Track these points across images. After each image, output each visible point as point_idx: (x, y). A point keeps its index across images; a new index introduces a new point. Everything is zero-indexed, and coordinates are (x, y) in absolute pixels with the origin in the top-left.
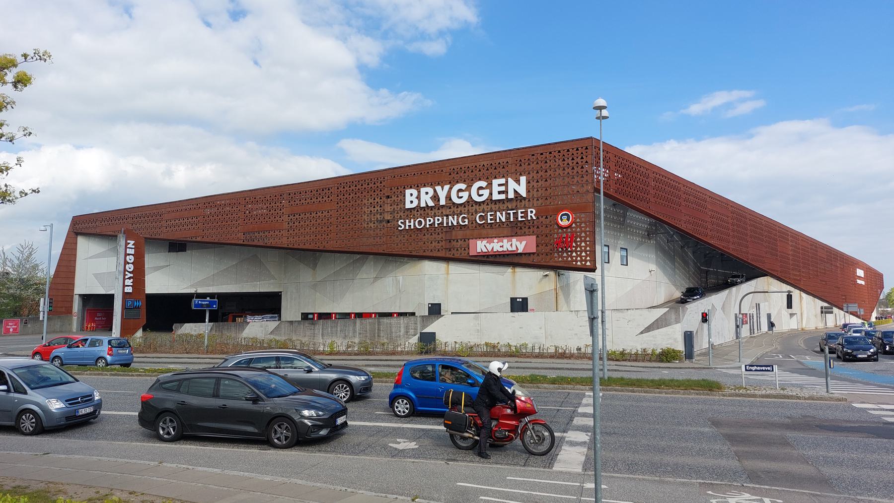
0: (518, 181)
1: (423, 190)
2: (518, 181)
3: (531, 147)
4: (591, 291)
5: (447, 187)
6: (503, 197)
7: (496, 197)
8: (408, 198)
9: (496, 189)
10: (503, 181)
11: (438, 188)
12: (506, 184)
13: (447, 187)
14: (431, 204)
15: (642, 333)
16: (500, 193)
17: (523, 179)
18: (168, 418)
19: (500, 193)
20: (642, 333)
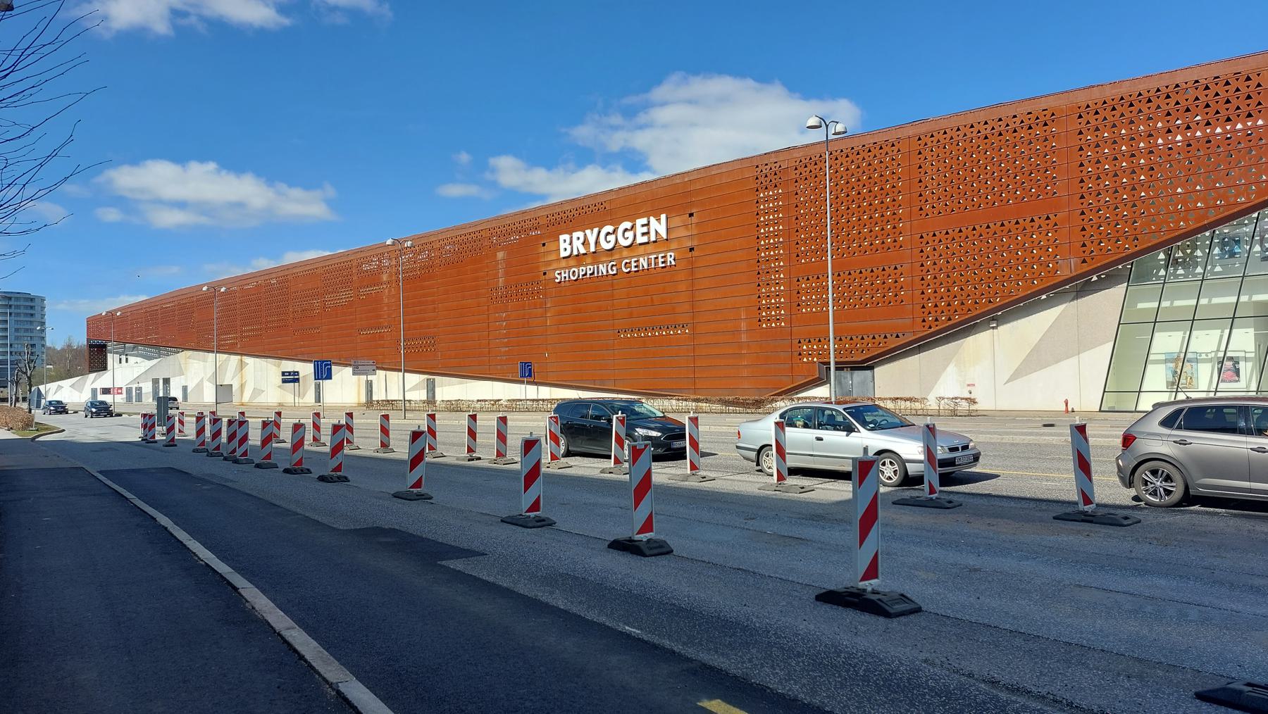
0: (659, 220)
1: (575, 235)
2: (659, 220)
3: (807, 146)
4: (444, 444)
5: (596, 230)
6: (645, 239)
7: (641, 239)
8: (562, 246)
9: (640, 230)
10: (644, 221)
11: (588, 232)
12: (648, 225)
13: (596, 230)
14: (583, 251)
15: (1008, 381)
16: (643, 234)
17: (663, 217)
18: (887, 461)
19: (643, 234)
20: (1008, 381)
